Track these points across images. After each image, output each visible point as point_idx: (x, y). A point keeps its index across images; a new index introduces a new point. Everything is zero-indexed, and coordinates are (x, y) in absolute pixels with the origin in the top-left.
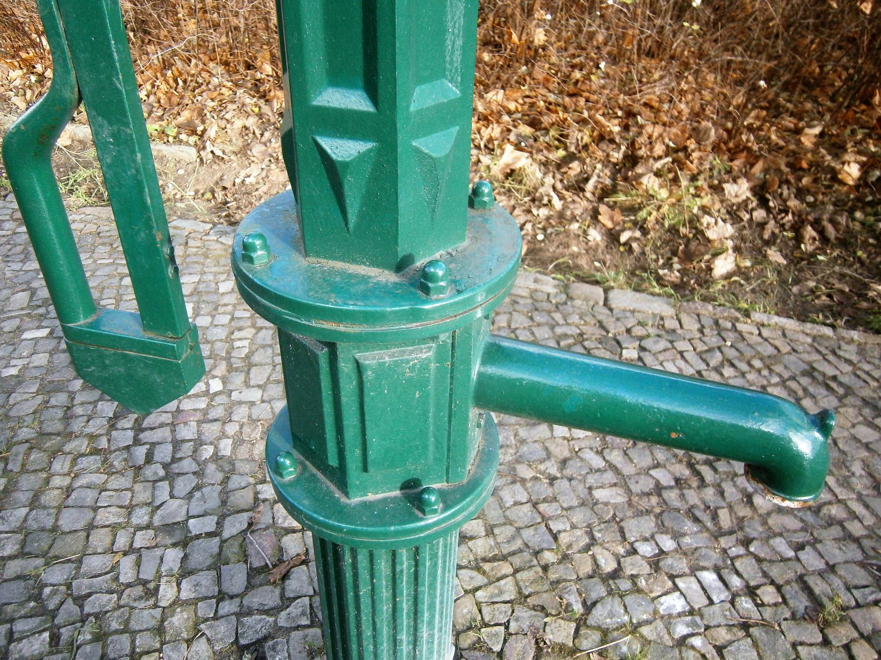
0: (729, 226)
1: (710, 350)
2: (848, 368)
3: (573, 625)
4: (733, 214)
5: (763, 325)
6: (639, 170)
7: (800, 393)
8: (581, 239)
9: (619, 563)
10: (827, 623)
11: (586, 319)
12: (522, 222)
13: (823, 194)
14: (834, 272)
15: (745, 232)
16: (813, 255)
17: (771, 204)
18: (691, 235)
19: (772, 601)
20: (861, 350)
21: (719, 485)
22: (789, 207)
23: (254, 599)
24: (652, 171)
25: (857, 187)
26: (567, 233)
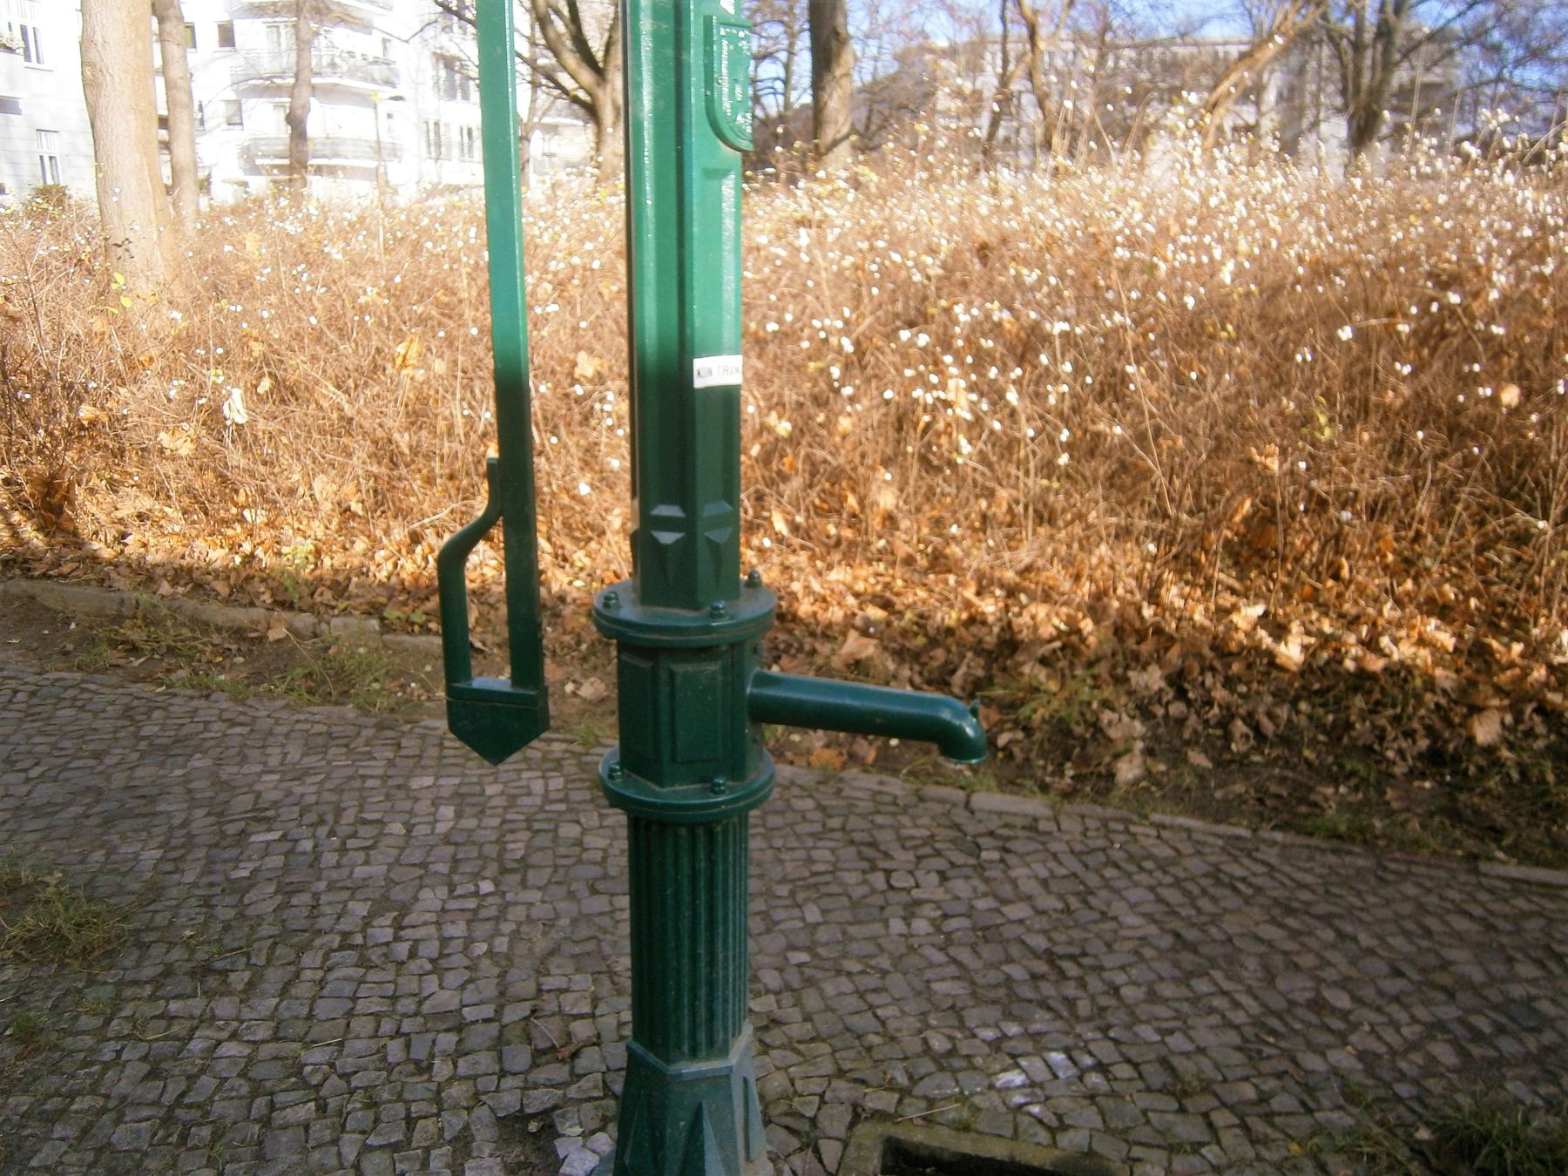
2: (1260, 869)
4: (1143, 710)
6: (1020, 657)
16: (1246, 755)
17: (1191, 695)
23: (540, 1075)
25: (1302, 673)
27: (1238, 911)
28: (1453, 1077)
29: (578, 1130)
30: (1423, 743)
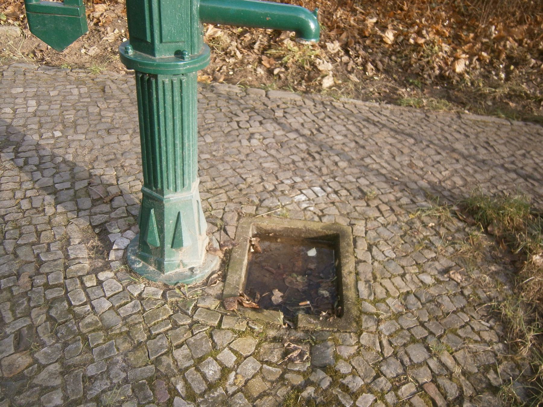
0: (330, 64)
1: (319, 112)
2: (385, 118)
3: (255, 207)
4: (332, 59)
5: (346, 103)
6: (282, 37)
7: (362, 127)
8: (253, 73)
9: (275, 187)
10: (368, 200)
11: (257, 102)
12: (221, 66)
13: (377, 48)
14: (382, 85)
15: (338, 67)
16: (372, 77)
17: (351, 53)
18: (311, 69)
19: (345, 194)
20: (392, 112)
21: (322, 160)
22: (359, 54)
23: (97, 209)
24: (289, 37)
25: (393, 45)
26: (245, 70)
27: (378, 132)
28: (462, 188)
29: (118, 230)
30: (437, 72)
